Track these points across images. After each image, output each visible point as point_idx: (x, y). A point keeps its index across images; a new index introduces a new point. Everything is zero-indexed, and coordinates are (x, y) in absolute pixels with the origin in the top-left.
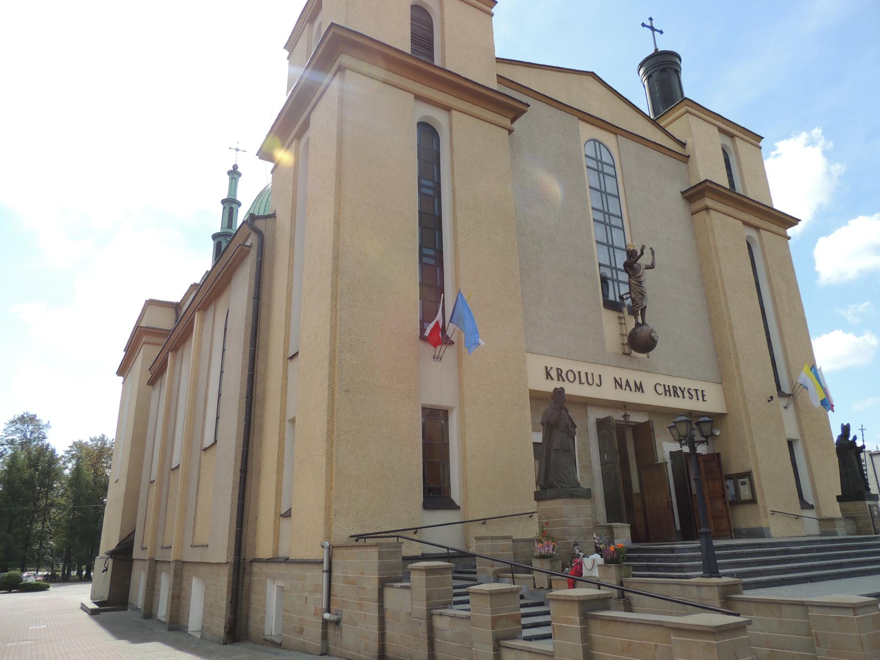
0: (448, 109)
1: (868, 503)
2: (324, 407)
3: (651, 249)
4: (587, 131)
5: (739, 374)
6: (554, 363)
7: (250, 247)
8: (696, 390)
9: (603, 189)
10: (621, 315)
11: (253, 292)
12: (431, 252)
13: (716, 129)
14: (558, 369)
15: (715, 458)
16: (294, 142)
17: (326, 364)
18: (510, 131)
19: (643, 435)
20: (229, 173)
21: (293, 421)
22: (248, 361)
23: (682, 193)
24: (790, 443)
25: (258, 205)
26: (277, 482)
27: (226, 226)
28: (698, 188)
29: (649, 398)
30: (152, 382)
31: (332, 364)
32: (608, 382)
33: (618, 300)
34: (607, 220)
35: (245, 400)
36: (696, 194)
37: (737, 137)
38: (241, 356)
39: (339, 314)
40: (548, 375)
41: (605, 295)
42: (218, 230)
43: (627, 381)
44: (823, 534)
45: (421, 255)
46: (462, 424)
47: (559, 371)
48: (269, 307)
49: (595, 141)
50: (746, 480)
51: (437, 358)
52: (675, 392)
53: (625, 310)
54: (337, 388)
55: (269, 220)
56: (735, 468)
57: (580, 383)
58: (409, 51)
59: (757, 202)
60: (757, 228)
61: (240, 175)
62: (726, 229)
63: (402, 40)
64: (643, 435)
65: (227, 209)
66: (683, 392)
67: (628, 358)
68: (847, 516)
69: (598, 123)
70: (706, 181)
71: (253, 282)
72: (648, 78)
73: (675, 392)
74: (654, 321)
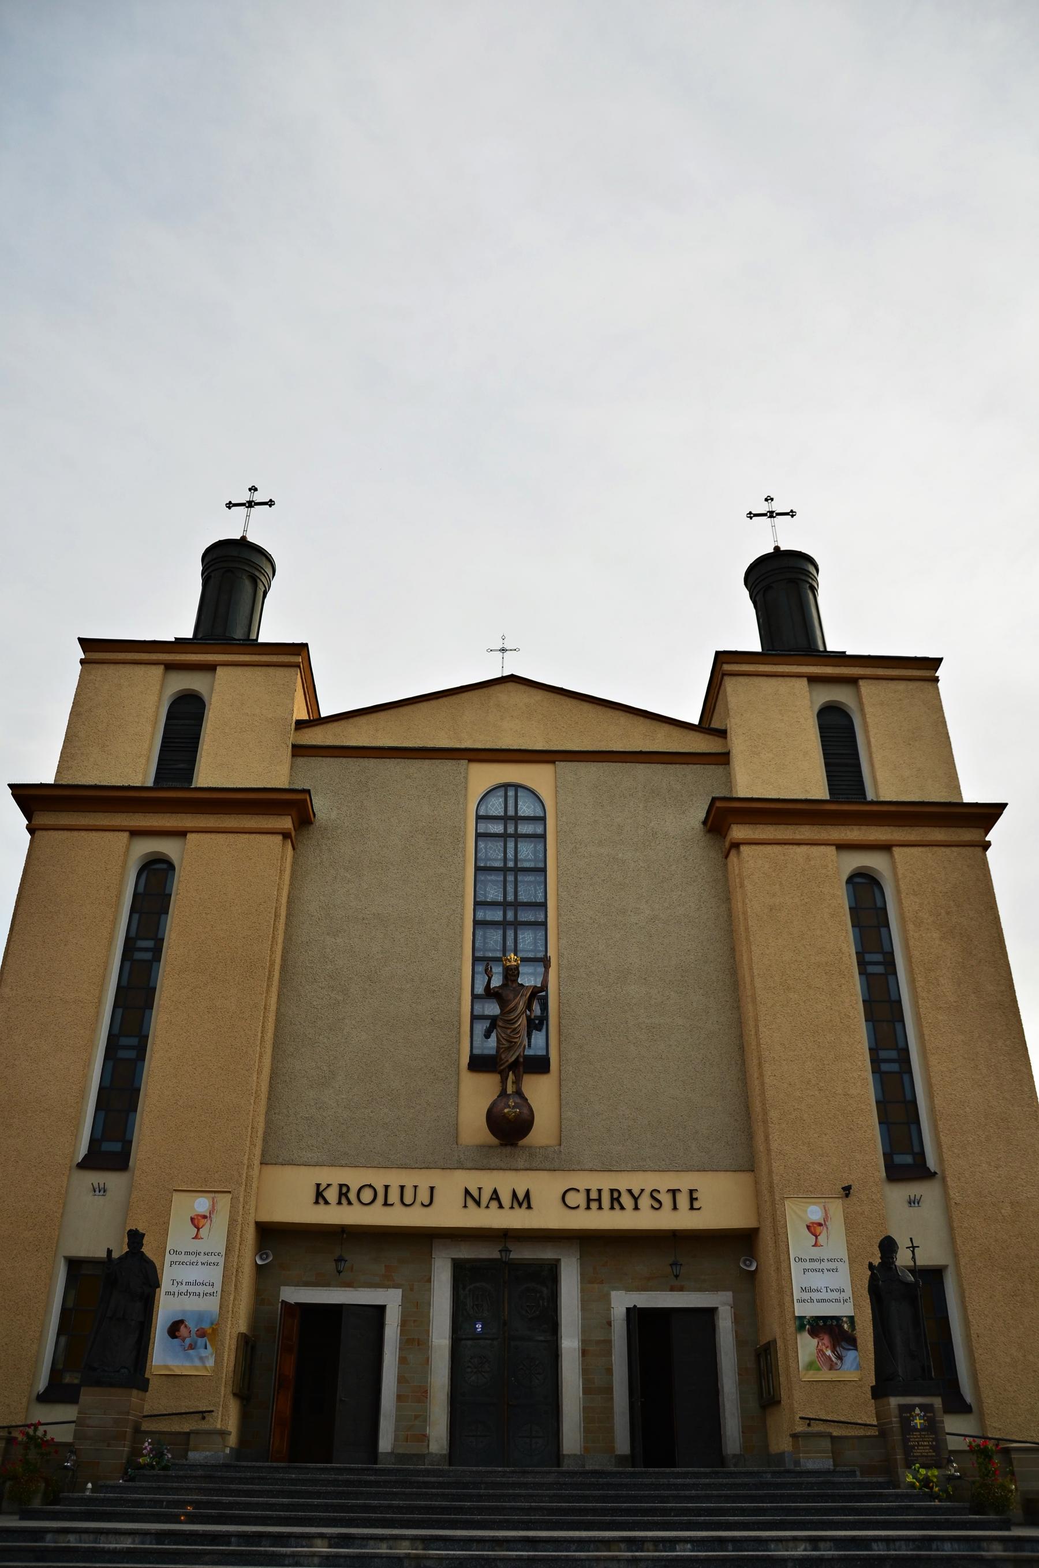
0: (886, 848)
4: (484, 777)
6: (333, 1177)
8: (674, 1192)
29: (547, 1215)
40: (320, 1196)
47: (343, 1192)
49: (506, 786)
51: (913, 1202)
57: (386, 1204)
66: (636, 1200)
69: (502, 756)
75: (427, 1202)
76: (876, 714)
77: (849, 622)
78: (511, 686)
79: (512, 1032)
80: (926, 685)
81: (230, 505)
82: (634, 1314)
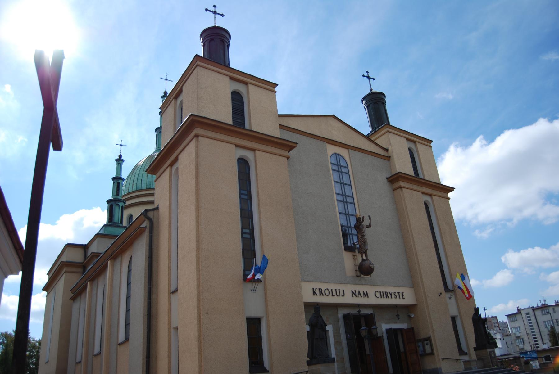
0: (254, 150)
1: (488, 350)
2: (196, 322)
3: (369, 216)
4: (331, 150)
5: (422, 282)
6: (317, 286)
7: (145, 228)
8: (399, 293)
9: (342, 182)
10: (354, 254)
11: (148, 254)
12: (245, 192)
13: (405, 140)
14: (319, 289)
15: (411, 330)
16: (169, 168)
17: (195, 299)
18: (288, 158)
19: (370, 320)
20: (117, 160)
21: (177, 329)
22: (147, 294)
23: (387, 178)
24: (453, 319)
25: (133, 176)
26: (169, 363)
27: (115, 194)
28: (395, 176)
29: (372, 300)
30: (73, 299)
31: (198, 299)
32: (348, 294)
33: (353, 245)
34: (345, 199)
35: (146, 317)
36: (395, 179)
37: (417, 144)
38: (143, 292)
39: (201, 272)
40: (314, 293)
41: (345, 243)
42: (110, 197)
43: (359, 292)
44: (466, 369)
45: (240, 194)
46: (268, 326)
48: (158, 261)
49: (336, 154)
50: (428, 342)
51: (253, 290)
52: (386, 295)
53: (357, 251)
54: (202, 312)
55: (155, 211)
56: (423, 336)
57: (333, 295)
58: (230, 122)
59: (429, 181)
60: (431, 195)
61: (123, 161)
62: (413, 198)
63: (227, 117)
64: (370, 320)
65: (116, 184)
66: (391, 295)
67: (359, 278)
68: (480, 359)
70: (399, 172)
71: (148, 248)
72: (368, 107)
73: (386, 295)
74: (373, 257)
75: (377, 293)
76: (254, 97)
77: (239, 58)
78: (332, 118)
79: (354, 236)
80: (270, 93)
81: (223, 15)
82: (387, 330)
